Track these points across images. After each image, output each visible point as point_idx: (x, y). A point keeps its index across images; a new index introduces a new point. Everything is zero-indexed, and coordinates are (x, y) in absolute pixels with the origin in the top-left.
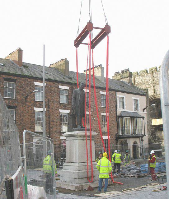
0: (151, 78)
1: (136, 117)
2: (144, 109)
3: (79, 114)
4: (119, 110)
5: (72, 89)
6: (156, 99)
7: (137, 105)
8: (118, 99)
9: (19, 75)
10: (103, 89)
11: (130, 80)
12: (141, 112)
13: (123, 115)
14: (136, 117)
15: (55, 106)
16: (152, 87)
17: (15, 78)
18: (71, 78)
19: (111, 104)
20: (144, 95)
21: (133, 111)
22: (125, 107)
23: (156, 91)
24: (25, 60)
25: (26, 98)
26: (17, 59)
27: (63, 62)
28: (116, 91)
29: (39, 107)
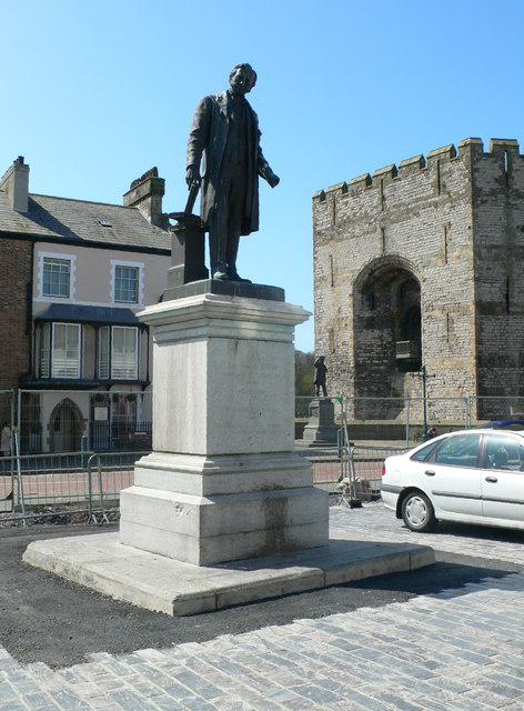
0: (376, 201)
16: (379, 230)
21: (112, 305)
22: (73, 290)
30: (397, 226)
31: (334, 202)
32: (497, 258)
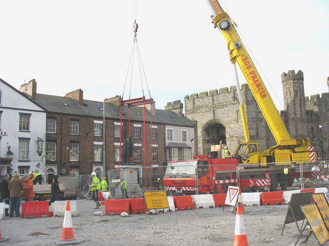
0: (211, 101)
1: (183, 148)
2: (192, 140)
3: (128, 155)
4: (167, 142)
5: (125, 125)
6: (216, 124)
7: (185, 136)
8: (166, 131)
9: (82, 115)
10: (154, 123)
11: (181, 111)
12: (188, 143)
13: (170, 146)
14: (183, 148)
15: (111, 140)
16: (212, 111)
17: (79, 118)
18: (124, 115)
19: (160, 136)
20: (193, 127)
21: (181, 142)
22: (173, 138)
23: (216, 114)
24: (86, 97)
25: (87, 134)
26: (78, 99)
27: (117, 99)
28: (165, 124)
29: (98, 141)
30: (219, 110)
31: (194, 100)
32: (254, 121)
